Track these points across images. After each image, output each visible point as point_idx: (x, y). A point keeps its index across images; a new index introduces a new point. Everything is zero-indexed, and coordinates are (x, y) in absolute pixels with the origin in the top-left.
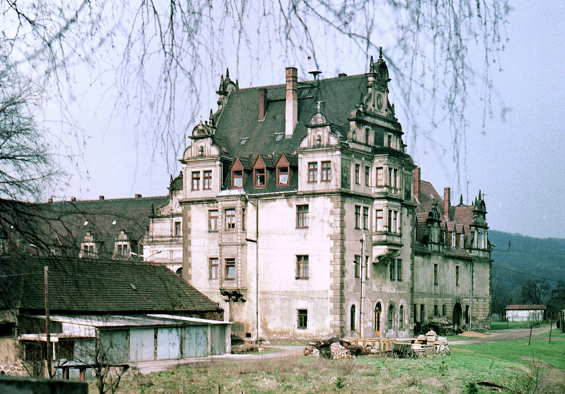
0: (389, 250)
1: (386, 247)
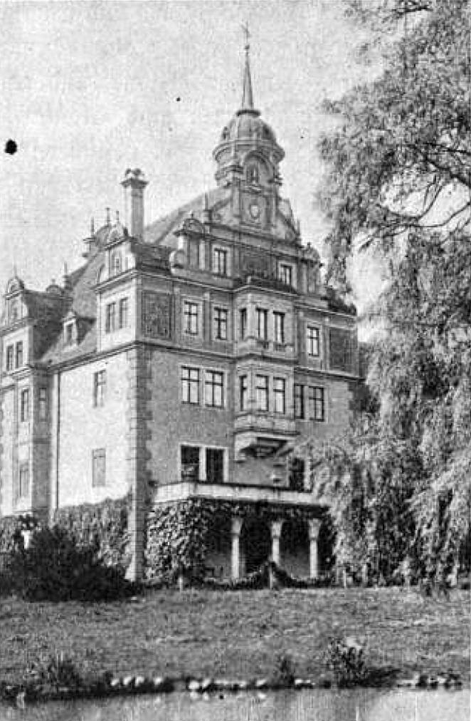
0: (259, 439)
1: (249, 434)
